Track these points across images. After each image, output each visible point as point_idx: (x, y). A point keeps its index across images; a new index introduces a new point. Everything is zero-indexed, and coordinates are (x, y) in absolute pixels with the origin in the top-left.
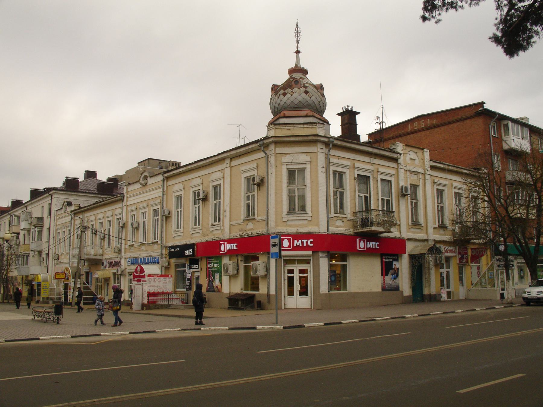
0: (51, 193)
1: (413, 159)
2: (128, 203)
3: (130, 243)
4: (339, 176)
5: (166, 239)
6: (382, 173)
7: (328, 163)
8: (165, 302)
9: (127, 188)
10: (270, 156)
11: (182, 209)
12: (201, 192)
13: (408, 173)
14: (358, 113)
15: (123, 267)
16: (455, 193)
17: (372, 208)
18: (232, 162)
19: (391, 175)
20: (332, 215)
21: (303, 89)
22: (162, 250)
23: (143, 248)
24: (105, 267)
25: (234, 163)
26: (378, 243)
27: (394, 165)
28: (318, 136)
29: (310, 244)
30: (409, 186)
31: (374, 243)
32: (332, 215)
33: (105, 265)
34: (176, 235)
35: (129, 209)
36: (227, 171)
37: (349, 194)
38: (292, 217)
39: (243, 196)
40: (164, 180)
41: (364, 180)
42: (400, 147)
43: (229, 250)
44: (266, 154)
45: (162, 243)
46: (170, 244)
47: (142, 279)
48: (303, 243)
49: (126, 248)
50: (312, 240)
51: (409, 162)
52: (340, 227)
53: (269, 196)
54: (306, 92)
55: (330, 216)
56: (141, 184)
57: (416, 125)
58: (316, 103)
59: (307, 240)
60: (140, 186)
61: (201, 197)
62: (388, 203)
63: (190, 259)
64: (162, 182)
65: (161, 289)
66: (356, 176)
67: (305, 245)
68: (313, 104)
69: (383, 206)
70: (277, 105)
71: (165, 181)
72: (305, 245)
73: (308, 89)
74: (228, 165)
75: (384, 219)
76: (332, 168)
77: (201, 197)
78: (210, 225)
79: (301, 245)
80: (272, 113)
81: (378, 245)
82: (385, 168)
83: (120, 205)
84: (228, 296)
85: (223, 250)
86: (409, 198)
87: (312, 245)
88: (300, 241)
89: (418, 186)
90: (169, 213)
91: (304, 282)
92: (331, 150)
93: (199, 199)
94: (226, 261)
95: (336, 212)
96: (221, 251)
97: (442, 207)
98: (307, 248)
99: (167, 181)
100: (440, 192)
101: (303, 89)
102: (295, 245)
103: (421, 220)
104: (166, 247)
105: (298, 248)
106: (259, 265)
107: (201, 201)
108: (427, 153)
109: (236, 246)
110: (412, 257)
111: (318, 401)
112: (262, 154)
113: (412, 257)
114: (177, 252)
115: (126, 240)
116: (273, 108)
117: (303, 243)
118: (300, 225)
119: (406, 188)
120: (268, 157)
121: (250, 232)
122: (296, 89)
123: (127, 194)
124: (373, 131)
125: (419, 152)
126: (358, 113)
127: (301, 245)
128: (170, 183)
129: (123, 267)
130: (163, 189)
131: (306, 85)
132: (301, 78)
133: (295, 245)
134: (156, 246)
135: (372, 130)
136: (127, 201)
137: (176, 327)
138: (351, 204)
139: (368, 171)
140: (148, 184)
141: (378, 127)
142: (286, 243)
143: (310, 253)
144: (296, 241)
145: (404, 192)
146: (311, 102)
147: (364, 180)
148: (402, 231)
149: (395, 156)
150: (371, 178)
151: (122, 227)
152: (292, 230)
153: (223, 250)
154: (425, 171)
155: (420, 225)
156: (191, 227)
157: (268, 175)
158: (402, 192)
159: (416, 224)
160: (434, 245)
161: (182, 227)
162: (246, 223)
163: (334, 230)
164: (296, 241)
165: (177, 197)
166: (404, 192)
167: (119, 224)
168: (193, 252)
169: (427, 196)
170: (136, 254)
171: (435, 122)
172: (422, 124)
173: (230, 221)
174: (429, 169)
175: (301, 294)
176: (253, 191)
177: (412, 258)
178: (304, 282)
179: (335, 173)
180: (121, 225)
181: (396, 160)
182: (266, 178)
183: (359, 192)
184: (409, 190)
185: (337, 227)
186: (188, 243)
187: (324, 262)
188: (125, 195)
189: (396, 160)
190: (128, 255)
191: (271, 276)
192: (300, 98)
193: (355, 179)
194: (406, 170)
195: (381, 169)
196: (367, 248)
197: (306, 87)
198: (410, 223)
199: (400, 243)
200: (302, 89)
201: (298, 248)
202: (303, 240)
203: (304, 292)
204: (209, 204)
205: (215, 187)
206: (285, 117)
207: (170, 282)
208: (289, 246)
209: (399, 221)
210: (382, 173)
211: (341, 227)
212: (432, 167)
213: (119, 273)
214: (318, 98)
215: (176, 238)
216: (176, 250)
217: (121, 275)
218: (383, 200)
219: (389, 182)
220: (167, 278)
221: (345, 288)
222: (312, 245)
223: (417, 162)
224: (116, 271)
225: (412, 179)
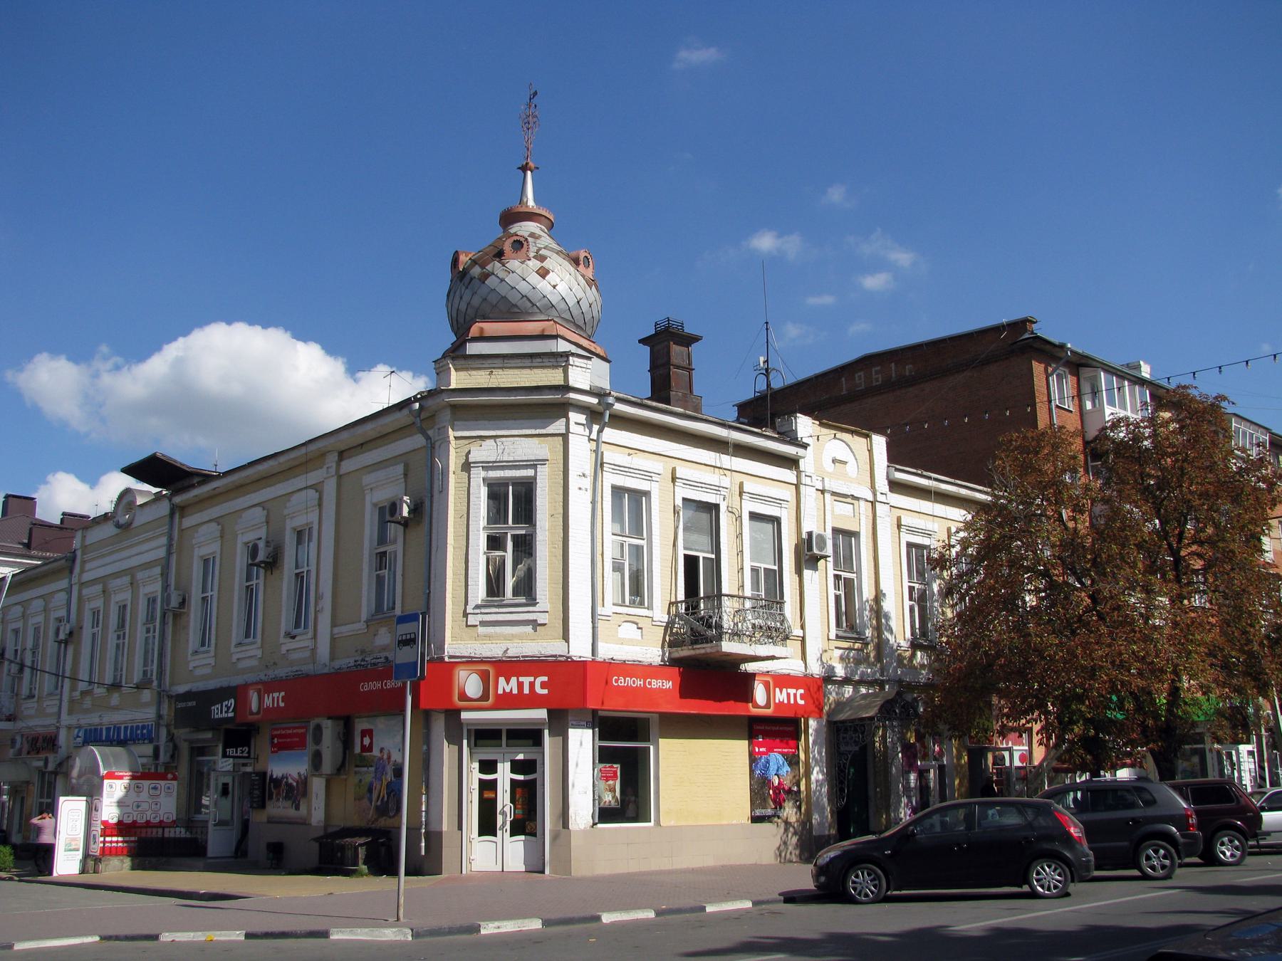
1: (841, 462)
2: (87, 577)
3: (82, 686)
6: (755, 497)
7: (600, 464)
9: (84, 537)
10: (437, 444)
11: (215, 593)
12: (261, 545)
13: (827, 496)
15: (63, 752)
16: (910, 545)
18: (343, 463)
19: (778, 501)
22: (159, 704)
23: (115, 699)
26: (802, 691)
29: (539, 690)
30: (829, 534)
31: (792, 691)
32: (607, 609)
34: (197, 663)
36: (330, 488)
40: (172, 514)
42: (805, 425)
43: (781, 703)
44: (428, 438)
45: (160, 685)
46: (182, 689)
48: (520, 685)
49: (72, 701)
50: (546, 679)
51: (829, 467)
52: (631, 642)
55: (600, 610)
56: (118, 526)
58: (572, 302)
59: (532, 679)
61: (261, 556)
62: (774, 579)
64: (167, 519)
65: (143, 812)
66: (679, 502)
67: (526, 691)
68: (563, 305)
69: (756, 585)
70: (463, 307)
71: (177, 516)
72: (526, 691)
73: (546, 264)
74: (333, 471)
77: (261, 556)
78: (282, 634)
79: (515, 691)
80: (452, 326)
81: (802, 697)
82: (767, 483)
83: (64, 584)
84: (321, 833)
85: (254, 707)
86: (830, 565)
87: (545, 691)
88: (514, 680)
90: (183, 603)
91: (527, 795)
92: (607, 430)
93: (258, 565)
96: (252, 713)
98: (530, 701)
99: (182, 517)
101: (534, 264)
104: (170, 697)
105: (507, 701)
107: (262, 571)
108: (880, 442)
109: (802, 697)
112: (418, 441)
117: (520, 685)
118: (511, 638)
119: (821, 539)
120: (433, 447)
121: (384, 654)
122: (514, 264)
123: (84, 553)
125: (859, 443)
127: (515, 691)
128: (188, 522)
129: (63, 752)
130: (171, 539)
132: (532, 235)
133: (500, 691)
134: (147, 695)
137: (28, 953)
139: (717, 489)
140: (134, 525)
143: (541, 714)
144: (502, 680)
145: (815, 551)
147: (631, 503)
151: (66, 642)
152: (493, 650)
153: (254, 707)
154: (875, 495)
156: (234, 642)
158: (810, 549)
160: (899, 694)
161: (213, 641)
165: (206, 561)
166: (815, 551)
170: (93, 719)
171: (908, 369)
172: (877, 377)
173: (334, 625)
174: (886, 488)
175: (517, 829)
177: (838, 730)
178: (527, 795)
179: (618, 491)
180: (62, 636)
182: (427, 503)
185: (622, 642)
188: (79, 553)
189: (791, 463)
190: (72, 720)
193: (676, 512)
196: (497, 696)
198: (833, 636)
200: (530, 263)
201: (507, 701)
202: (521, 679)
204: (282, 579)
205: (300, 534)
206: (482, 338)
207: (169, 794)
208: (485, 696)
209: (803, 627)
210: (912, 530)
212: (895, 486)
213: (51, 767)
217: (55, 773)
218: (755, 571)
219: (776, 521)
220: (163, 783)
221: (51, 873)
222: (545, 691)
223: (851, 468)
224: (41, 764)
225: (841, 515)
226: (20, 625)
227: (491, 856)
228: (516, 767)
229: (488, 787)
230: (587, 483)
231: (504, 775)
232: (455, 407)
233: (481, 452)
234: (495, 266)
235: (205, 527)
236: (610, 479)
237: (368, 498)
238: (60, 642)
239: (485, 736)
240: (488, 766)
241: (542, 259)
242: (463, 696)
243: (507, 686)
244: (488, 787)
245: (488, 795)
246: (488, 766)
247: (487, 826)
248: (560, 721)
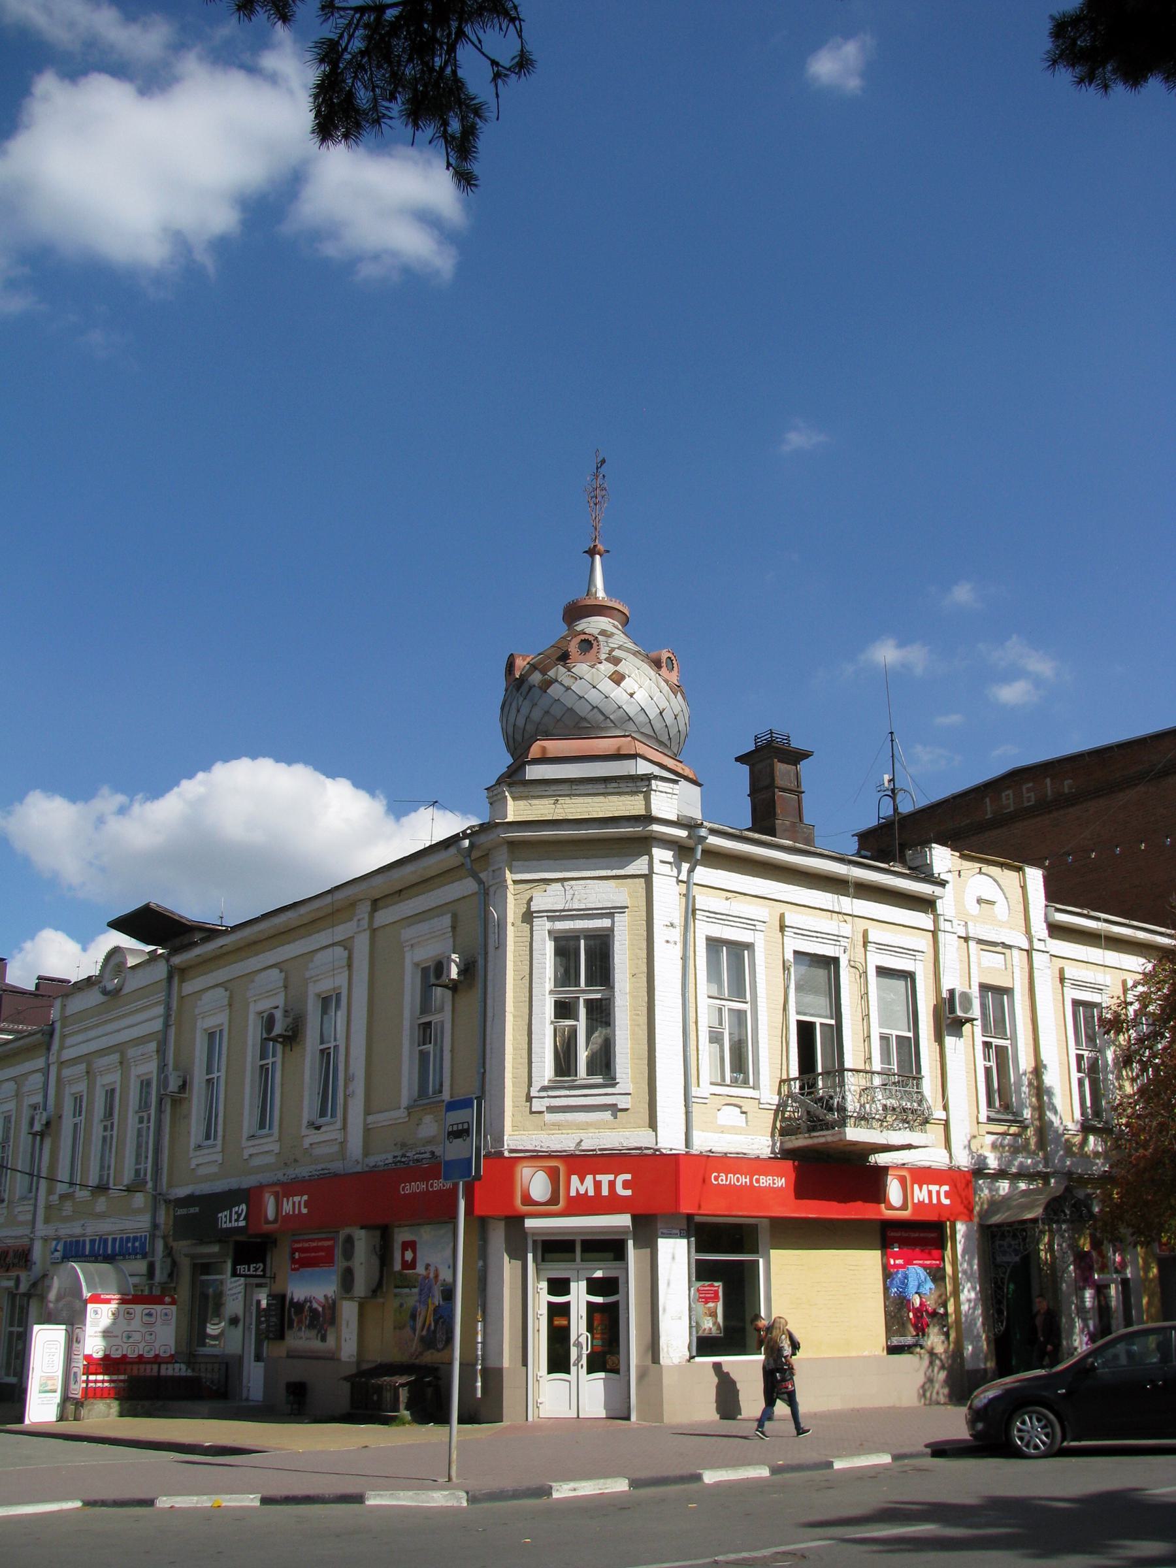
2: (68, 1054)
3: (61, 1188)
5: (170, 1174)
6: (883, 947)
7: (691, 912)
9: (64, 1006)
10: (492, 890)
12: (278, 1014)
13: (972, 944)
15: (37, 1269)
17: (847, 1065)
18: (377, 914)
19: (912, 952)
23: (101, 1204)
25: (385, 916)
27: (923, 920)
30: (975, 992)
32: (703, 1089)
35: (66, 1072)
36: (362, 945)
39: (407, 1024)
40: (170, 978)
42: (942, 858)
44: (480, 882)
45: (155, 1188)
46: (182, 1192)
48: (598, 1185)
49: (49, 1207)
50: (628, 1177)
51: (974, 908)
52: (733, 1130)
53: (489, 1023)
55: (695, 1091)
56: (105, 992)
57: (1008, 799)
58: (653, 713)
59: (611, 1177)
60: (101, 998)
61: (278, 1029)
62: (909, 1049)
63: (237, 1243)
66: (790, 956)
67: (605, 1192)
70: (521, 722)
71: (176, 980)
72: (605, 1192)
73: (621, 668)
75: (888, 1102)
76: (704, 929)
77: (278, 1029)
79: (591, 1193)
80: (509, 750)
82: (894, 931)
83: (40, 1063)
84: (354, 1371)
85: (271, 1213)
86: (978, 1030)
87: (629, 1193)
88: (589, 1178)
89: (1008, 991)
90: (183, 1087)
91: (607, 1321)
92: (699, 869)
93: (274, 1040)
96: (267, 1222)
98: (612, 1204)
99: (182, 981)
101: (606, 668)
102: (573, 1193)
105: (581, 1205)
107: (279, 1047)
112: (467, 886)
115: (52, 1179)
116: (510, 730)
117: (598, 1185)
119: (966, 997)
121: (429, 1148)
122: (581, 668)
124: (872, 822)
125: (1009, 878)
128: (189, 987)
130: (168, 1008)
131: (616, 653)
132: (603, 633)
133: (573, 1193)
134: (139, 1200)
135: (870, 822)
136: (62, 1048)
139: (836, 939)
141: (887, 810)
143: (624, 1220)
144: (575, 1179)
145: (959, 1013)
146: (632, 710)
150: (843, 963)
151: (42, 1134)
152: (564, 1142)
153: (271, 1213)
154: (1031, 942)
157: (486, 953)
160: (1068, 1189)
164: (575, 1179)
166: (959, 1013)
167: (32, 1124)
170: (73, 1229)
171: (1067, 785)
172: (1029, 796)
173: (368, 1112)
175: (594, 1366)
177: (993, 1236)
178: (607, 1321)
179: (714, 944)
180: (37, 1127)
182: (481, 962)
183: (798, 1013)
184: (976, 1003)
185: (723, 1130)
186: (235, 1186)
187: (675, 1255)
189: (926, 904)
190: (49, 1230)
193: (785, 968)
194: (966, 939)
200: (601, 667)
202: (598, 1177)
206: (544, 760)
208: (554, 1200)
210: (883, 947)
212: (1057, 930)
213: (23, 1288)
214: (657, 695)
215: (203, 1168)
217: (28, 1296)
218: (884, 1039)
220: (159, 1308)
222: (629, 1193)
223: (1001, 909)
224: (11, 1284)
225: (991, 967)
227: (564, 1398)
228: (594, 1287)
229: (558, 1312)
230: (676, 934)
231: (579, 1297)
232: (512, 844)
233: (548, 898)
236: (704, 929)
239: (555, 1248)
240: (559, 1286)
241: (616, 661)
242: (527, 1200)
244: (558, 1312)
245: (559, 1322)
246: (559, 1286)
247: (559, 1362)
248: (647, 1229)
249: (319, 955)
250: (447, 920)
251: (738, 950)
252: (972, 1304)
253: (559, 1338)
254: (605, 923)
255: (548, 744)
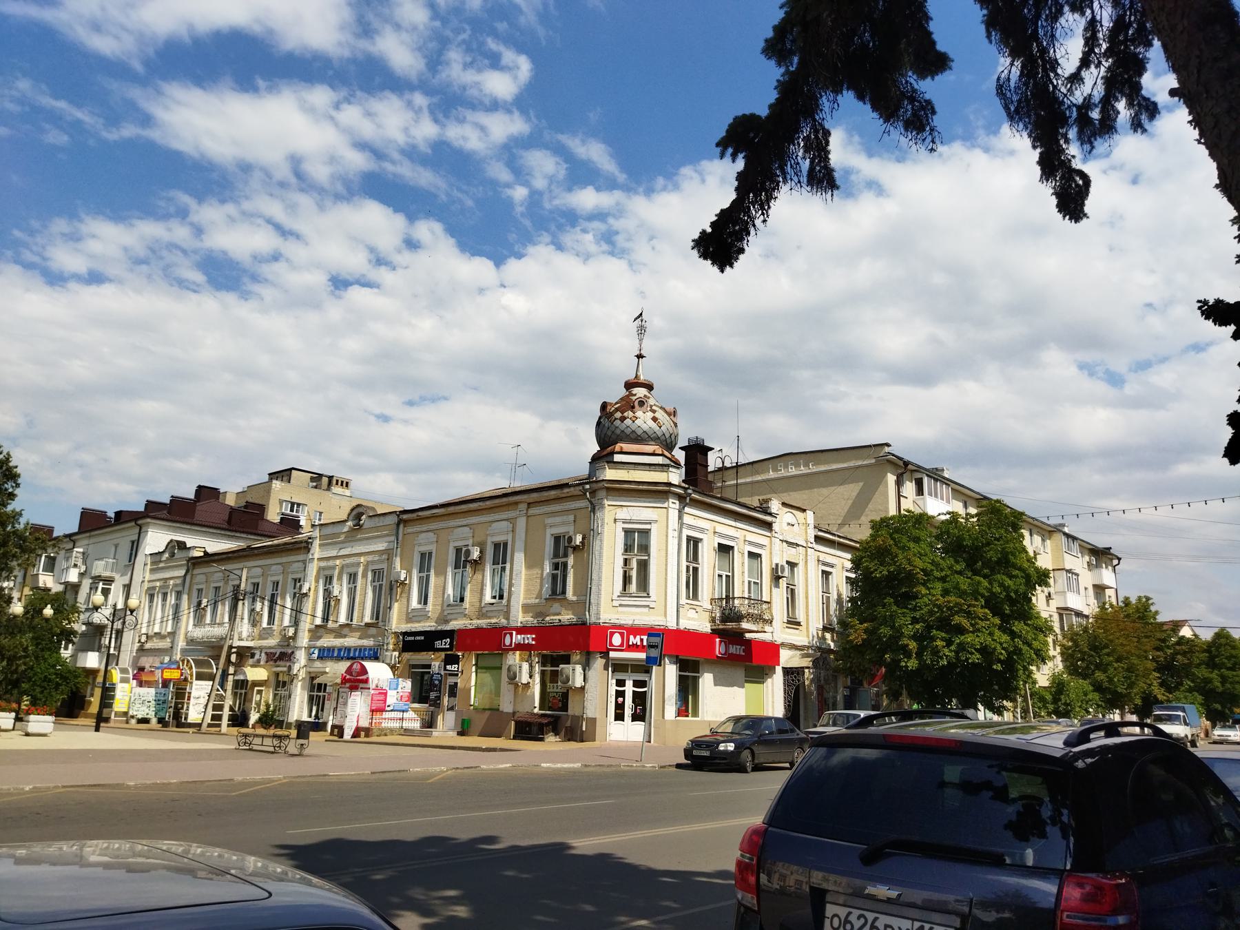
0: (140, 522)
4: (694, 543)
6: (751, 543)
8: (397, 725)
14: (712, 449)
20: (683, 600)
21: (650, 415)
24: (259, 661)
28: (669, 484)
32: (683, 600)
33: (257, 657)
37: (705, 571)
38: (627, 601)
40: (398, 525)
41: (725, 550)
47: (361, 685)
48: (642, 640)
52: (693, 619)
54: (655, 419)
73: (657, 415)
91: (640, 699)
94: (514, 659)
95: (688, 598)
97: (696, 570)
100: (826, 574)
101: (650, 415)
103: (801, 617)
106: (575, 673)
110: (787, 671)
111: (589, 908)
113: (787, 671)
114: (414, 643)
117: (642, 640)
122: (639, 413)
126: (712, 449)
138: (708, 587)
142: (617, 640)
147: (725, 550)
148: (777, 632)
149: (768, 518)
155: (799, 624)
159: (793, 623)
162: (550, 603)
163: (685, 624)
168: (451, 644)
169: (808, 581)
175: (636, 718)
176: (566, 555)
178: (640, 699)
179: (689, 538)
181: (768, 526)
187: (671, 671)
189: (768, 526)
191: (595, 686)
192: (645, 427)
195: (720, 528)
197: (654, 412)
199: (772, 650)
203: (638, 717)
205: (497, 546)
206: (622, 453)
208: (622, 645)
210: (825, 564)
211: (698, 620)
216: (418, 638)
221: (696, 714)
226: (280, 578)
227: (628, 732)
228: (637, 684)
229: (620, 694)
230: (676, 534)
231: (629, 688)
232: (608, 489)
233: (623, 514)
234: (629, 414)
235: (423, 535)
236: (686, 532)
237: (1060, 666)
238: (74, 542)
239: (619, 667)
240: (621, 683)
241: (654, 412)
242: (611, 644)
243: (633, 640)
244: (620, 694)
245: (620, 700)
246: (621, 683)
247: (619, 717)
248: (658, 661)
249: (495, 525)
250: (571, 518)
251: (758, 556)
252: (1106, 684)
253: (620, 707)
254: (647, 527)
255: (623, 445)
